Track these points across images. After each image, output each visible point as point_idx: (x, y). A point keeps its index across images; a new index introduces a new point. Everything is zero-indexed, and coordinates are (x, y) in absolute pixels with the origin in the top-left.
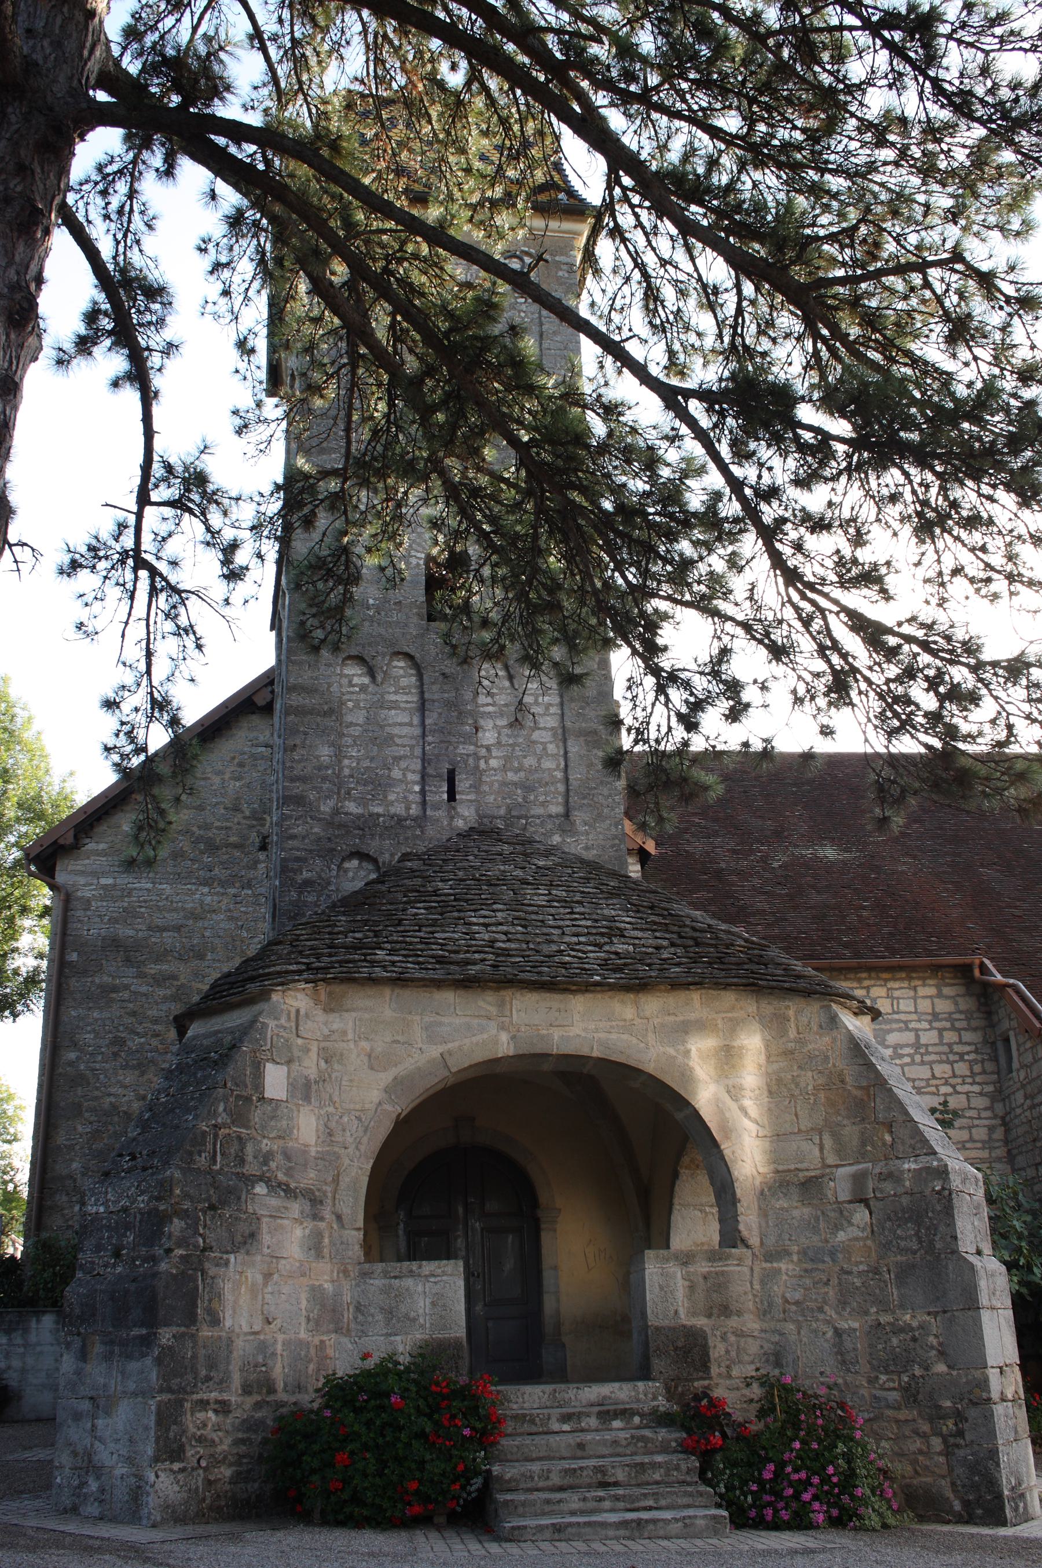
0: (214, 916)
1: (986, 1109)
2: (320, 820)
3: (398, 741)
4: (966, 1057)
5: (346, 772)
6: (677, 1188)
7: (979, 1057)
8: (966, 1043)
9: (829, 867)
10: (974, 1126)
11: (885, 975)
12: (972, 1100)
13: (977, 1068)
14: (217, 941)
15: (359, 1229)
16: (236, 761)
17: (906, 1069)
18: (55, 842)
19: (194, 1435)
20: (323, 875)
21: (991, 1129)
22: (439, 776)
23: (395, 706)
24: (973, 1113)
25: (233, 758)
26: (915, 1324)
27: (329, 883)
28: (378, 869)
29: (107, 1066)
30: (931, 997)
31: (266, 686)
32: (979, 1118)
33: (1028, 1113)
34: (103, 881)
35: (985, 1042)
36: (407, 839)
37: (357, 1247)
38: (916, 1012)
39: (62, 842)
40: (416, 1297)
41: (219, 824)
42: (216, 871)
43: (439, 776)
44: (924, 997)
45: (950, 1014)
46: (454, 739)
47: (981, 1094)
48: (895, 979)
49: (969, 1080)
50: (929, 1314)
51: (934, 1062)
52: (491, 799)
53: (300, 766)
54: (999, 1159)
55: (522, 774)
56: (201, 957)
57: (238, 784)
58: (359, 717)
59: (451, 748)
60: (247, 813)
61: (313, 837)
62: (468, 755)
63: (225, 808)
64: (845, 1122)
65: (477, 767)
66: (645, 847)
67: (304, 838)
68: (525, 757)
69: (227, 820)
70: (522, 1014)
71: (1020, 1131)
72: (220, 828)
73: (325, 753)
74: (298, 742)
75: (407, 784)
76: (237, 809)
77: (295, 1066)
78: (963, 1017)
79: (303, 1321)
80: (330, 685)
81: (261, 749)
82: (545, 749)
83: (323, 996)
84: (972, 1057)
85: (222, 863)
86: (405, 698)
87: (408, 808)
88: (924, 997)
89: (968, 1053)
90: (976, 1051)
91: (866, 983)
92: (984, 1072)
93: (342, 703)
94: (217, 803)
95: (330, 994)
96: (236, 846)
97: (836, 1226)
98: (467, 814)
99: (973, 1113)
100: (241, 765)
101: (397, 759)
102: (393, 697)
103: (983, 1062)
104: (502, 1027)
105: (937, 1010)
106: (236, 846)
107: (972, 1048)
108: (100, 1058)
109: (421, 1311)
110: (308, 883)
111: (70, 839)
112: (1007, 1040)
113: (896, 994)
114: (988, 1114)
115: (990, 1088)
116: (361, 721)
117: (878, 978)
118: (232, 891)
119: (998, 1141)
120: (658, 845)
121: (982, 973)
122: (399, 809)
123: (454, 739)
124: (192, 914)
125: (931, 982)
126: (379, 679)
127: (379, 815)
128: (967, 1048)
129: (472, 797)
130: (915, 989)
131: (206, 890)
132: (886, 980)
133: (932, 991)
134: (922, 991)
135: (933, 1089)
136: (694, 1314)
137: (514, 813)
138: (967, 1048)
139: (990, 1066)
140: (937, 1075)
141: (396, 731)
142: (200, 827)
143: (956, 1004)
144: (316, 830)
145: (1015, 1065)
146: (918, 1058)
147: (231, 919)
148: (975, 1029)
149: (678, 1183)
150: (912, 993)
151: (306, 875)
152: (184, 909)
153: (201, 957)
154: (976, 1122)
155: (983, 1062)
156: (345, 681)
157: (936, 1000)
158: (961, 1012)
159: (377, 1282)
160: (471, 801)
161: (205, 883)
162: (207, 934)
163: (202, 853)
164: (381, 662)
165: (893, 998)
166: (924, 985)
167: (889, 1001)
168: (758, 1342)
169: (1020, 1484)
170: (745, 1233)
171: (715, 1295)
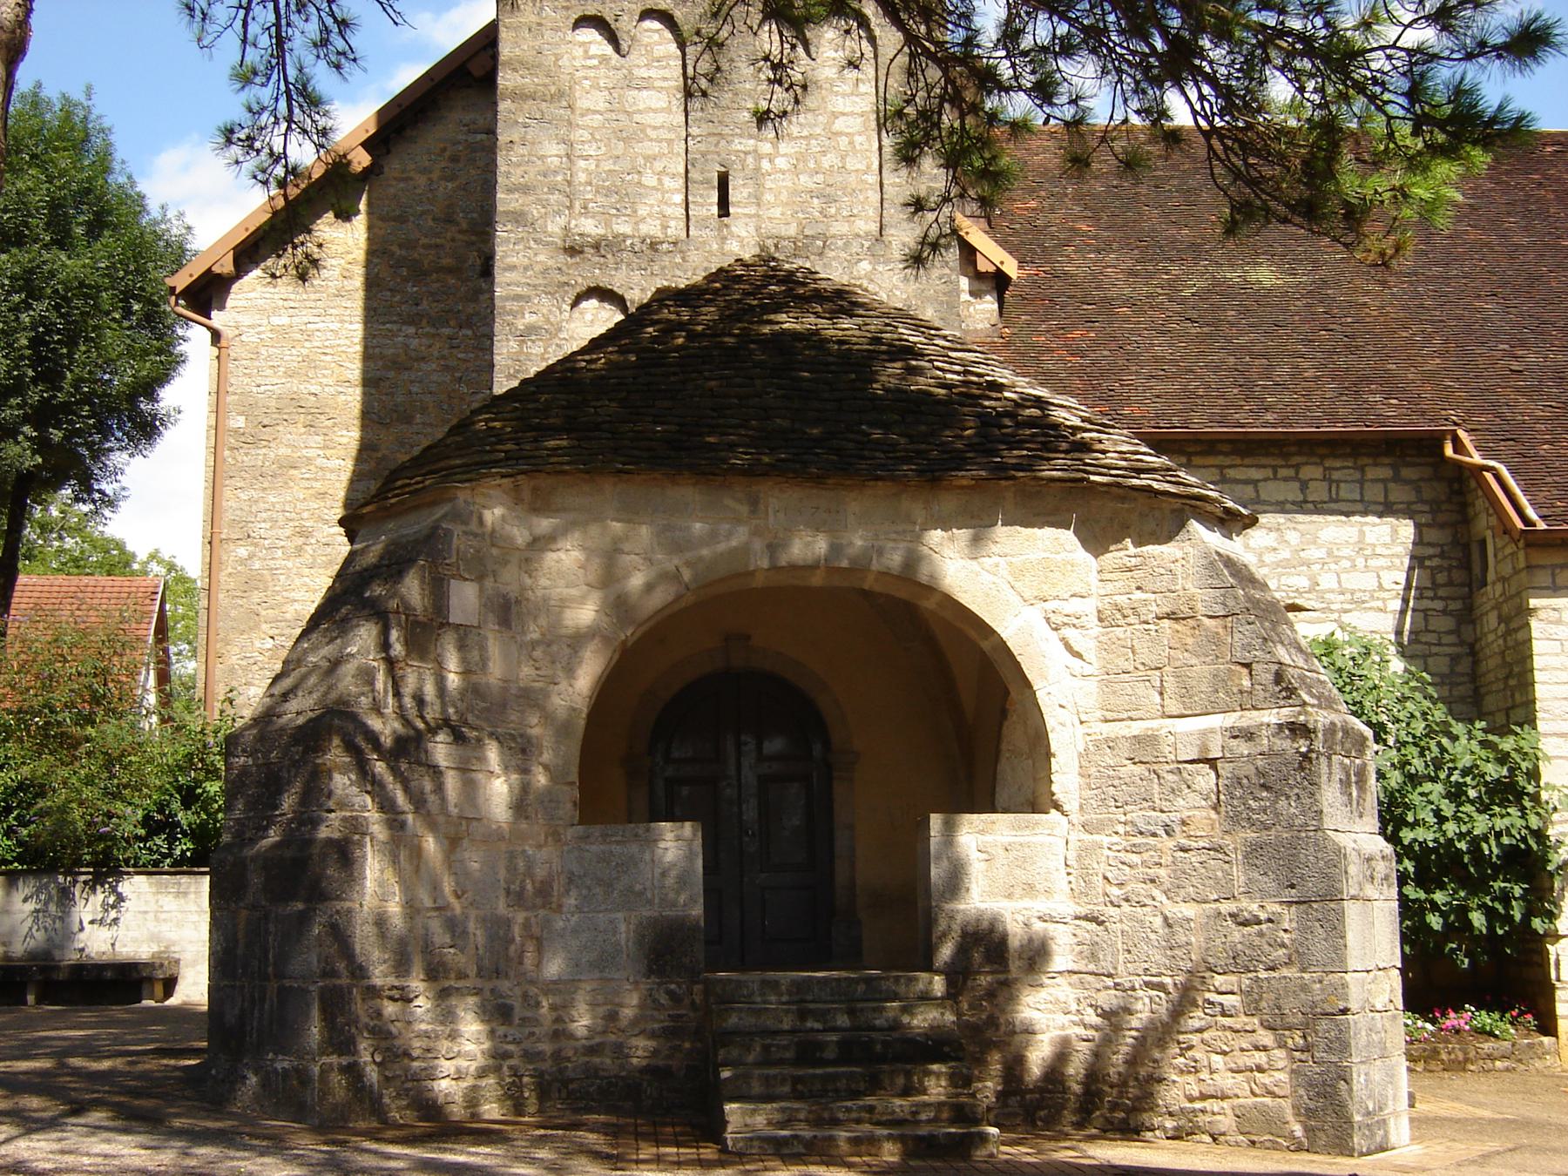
0: (423, 366)
1: (1449, 632)
2: (548, 244)
3: (652, 134)
4: (1427, 563)
5: (582, 177)
6: (1005, 731)
7: (1445, 563)
8: (1429, 544)
9: (1263, 296)
10: (1430, 655)
11: (1322, 451)
12: (1432, 621)
13: (1441, 578)
14: (428, 398)
15: (572, 783)
16: (447, 154)
17: (1343, 576)
18: (209, 270)
19: (366, 1026)
20: (552, 319)
21: (1455, 659)
22: (708, 181)
23: (645, 85)
24: (1431, 638)
25: (444, 150)
26: (1263, 916)
27: (560, 330)
28: (624, 309)
29: (290, 564)
30: (1384, 481)
31: (484, 48)
32: (1439, 645)
33: (1501, 641)
34: (275, 320)
35: (1455, 542)
36: (663, 268)
37: (569, 806)
38: (1362, 501)
39: (217, 269)
40: (642, 866)
41: (424, 241)
42: (425, 305)
43: (708, 181)
44: (1372, 481)
45: (1410, 503)
46: (726, 131)
47: (1444, 612)
48: (1335, 456)
49: (1430, 594)
50: (1281, 903)
51: (1383, 568)
52: (776, 212)
53: (519, 171)
54: (1462, 699)
55: (820, 178)
56: (408, 420)
57: (450, 185)
58: (598, 101)
59: (723, 143)
60: (464, 226)
61: (537, 268)
62: (746, 153)
63: (434, 219)
64: (1194, 661)
65: (757, 169)
66: (1004, 268)
67: (526, 269)
68: (824, 153)
69: (437, 235)
70: (781, 515)
71: (1492, 663)
72: (428, 247)
73: (552, 150)
74: (515, 137)
75: (664, 192)
76: (449, 220)
77: (489, 583)
78: (1426, 508)
79: (502, 893)
80: (558, 57)
81: (479, 137)
82: (851, 143)
83: (526, 494)
84: (1435, 562)
85: (431, 294)
86: (662, 73)
87: (665, 227)
88: (1372, 481)
89: (1430, 557)
90: (1442, 555)
91: (1296, 460)
92: (1450, 583)
93: (574, 81)
94: (423, 213)
95: (535, 490)
96: (450, 271)
97: (1173, 791)
98: (744, 234)
99: (1431, 638)
100: (454, 159)
101: (651, 159)
102: (644, 73)
103: (1450, 569)
104: (756, 532)
105: (1392, 498)
106: (450, 271)
107: (1437, 550)
108: (280, 552)
109: (648, 884)
110: (531, 330)
111: (227, 267)
112: (1483, 543)
113: (1336, 475)
114: (1451, 639)
115: (1455, 606)
116: (602, 106)
117: (1312, 454)
118: (446, 331)
119: (1462, 675)
120: (1022, 262)
121: (1455, 451)
122: (651, 228)
123: (726, 131)
124: (394, 362)
125: (1387, 461)
126: (624, 46)
127: (626, 237)
128: (1431, 551)
129: (752, 210)
130: (1362, 469)
131: (411, 330)
132: (1323, 457)
133: (1384, 472)
134: (1372, 473)
135: (1379, 604)
136: (991, 894)
137: (807, 232)
138: (1431, 551)
139: (1458, 576)
140: (1386, 586)
141: (649, 119)
142: (400, 246)
143: (1418, 491)
144: (541, 258)
145: (1491, 576)
146: (1360, 562)
147: (447, 368)
148: (1442, 526)
149: (1006, 724)
150: (1357, 475)
151: (529, 319)
152: (382, 357)
153: (408, 420)
154: (1435, 649)
155: (1450, 569)
156: (579, 52)
157: (1391, 485)
158: (1422, 502)
159: (594, 848)
160: (749, 216)
161: (413, 320)
162: (415, 389)
163: (405, 280)
164: (625, 25)
165: (1331, 481)
166: (1376, 465)
167: (1325, 484)
168: (1069, 929)
169: (1381, 1109)
170: (1059, 796)
171: (1018, 872)
